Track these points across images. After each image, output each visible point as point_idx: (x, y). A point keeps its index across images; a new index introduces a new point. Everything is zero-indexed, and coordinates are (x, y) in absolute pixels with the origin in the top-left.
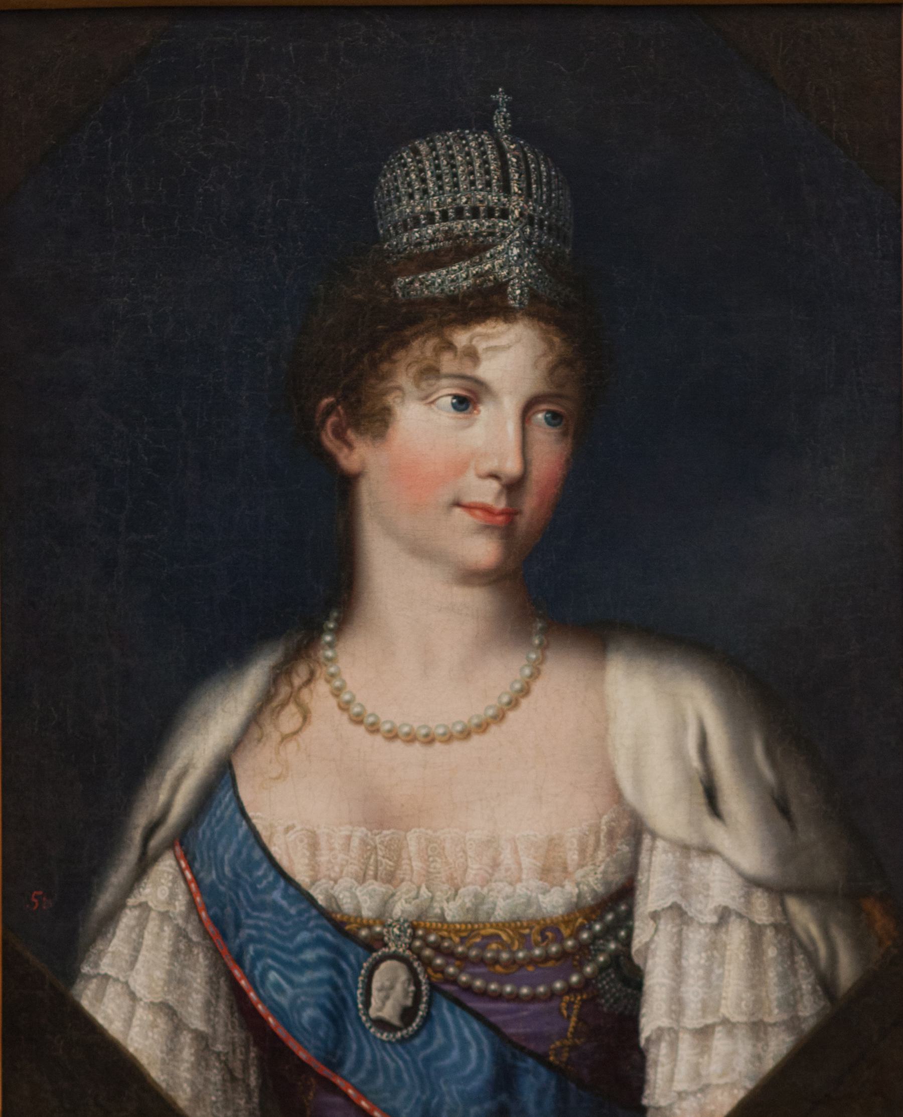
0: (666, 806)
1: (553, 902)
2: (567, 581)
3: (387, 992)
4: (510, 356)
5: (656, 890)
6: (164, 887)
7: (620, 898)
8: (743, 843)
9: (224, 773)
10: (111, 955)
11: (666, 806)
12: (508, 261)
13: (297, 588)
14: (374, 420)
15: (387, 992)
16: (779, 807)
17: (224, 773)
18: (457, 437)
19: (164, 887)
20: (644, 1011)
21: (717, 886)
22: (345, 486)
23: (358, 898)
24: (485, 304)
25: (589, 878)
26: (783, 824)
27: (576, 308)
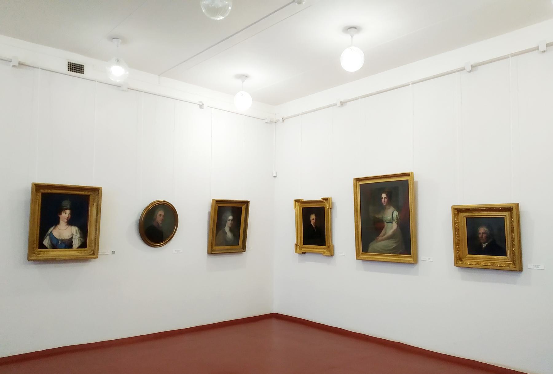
0: (75, 233)
1: (68, 238)
2: (70, 222)
3: (60, 242)
4: (68, 211)
5: (74, 237)
6: (48, 237)
7: (72, 238)
8: (78, 235)
9: (51, 232)
10: (45, 241)
11: (75, 233)
12: (68, 207)
13: (56, 222)
14: (61, 214)
15: (60, 242)
16: (80, 234)
17: (51, 232)
18: (65, 215)
19: (48, 237)
20: (29, 206)
21: (77, 237)
22: (59, 217)
23: (58, 238)
24: (67, 209)
25: (70, 237)
26: (306, 254)
27: (71, 209)
